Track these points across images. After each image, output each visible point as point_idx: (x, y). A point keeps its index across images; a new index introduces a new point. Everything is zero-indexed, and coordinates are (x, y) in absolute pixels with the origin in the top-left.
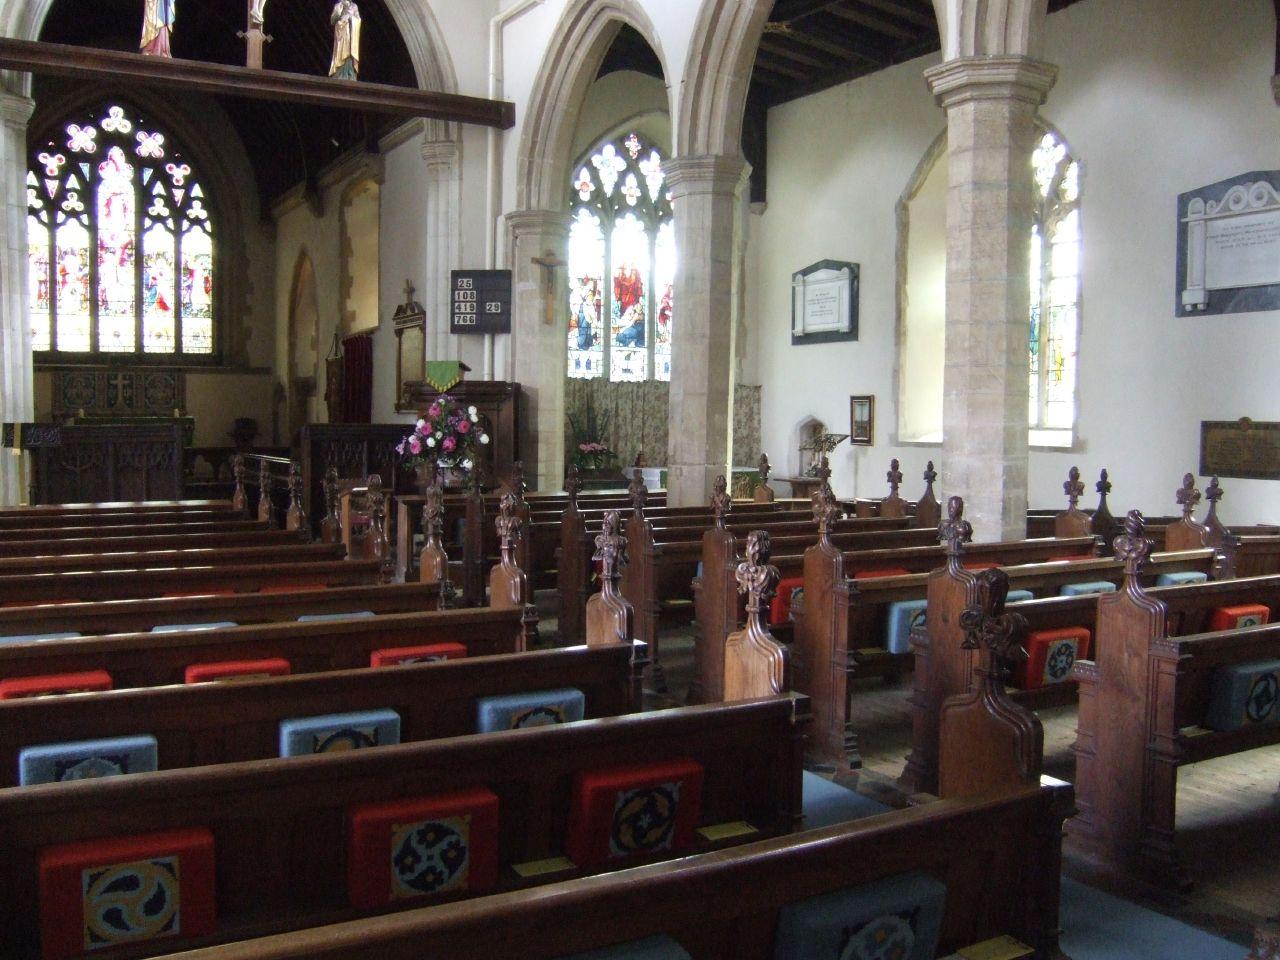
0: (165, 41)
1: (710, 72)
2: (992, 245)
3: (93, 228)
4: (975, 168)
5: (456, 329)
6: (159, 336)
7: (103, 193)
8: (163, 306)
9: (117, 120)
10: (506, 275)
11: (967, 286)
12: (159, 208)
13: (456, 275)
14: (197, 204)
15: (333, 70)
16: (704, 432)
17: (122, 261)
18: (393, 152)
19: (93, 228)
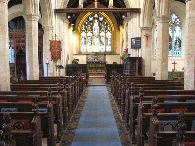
0: (82, 5)
1: (147, 3)
2: (193, 30)
3: (92, 33)
4: (189, 14)
5: (132, 48)
6: (103, 49)
7: (94, 27)
9: (96, 16)
10: (140, 38)
11: (187, 39)
12: (102, 29)
13: (132, 39)
14: (108, 28)
15: (109, 6)
16: (161, 66)
17: (97, 38)
18: (69, 24)
19: (92, 33)
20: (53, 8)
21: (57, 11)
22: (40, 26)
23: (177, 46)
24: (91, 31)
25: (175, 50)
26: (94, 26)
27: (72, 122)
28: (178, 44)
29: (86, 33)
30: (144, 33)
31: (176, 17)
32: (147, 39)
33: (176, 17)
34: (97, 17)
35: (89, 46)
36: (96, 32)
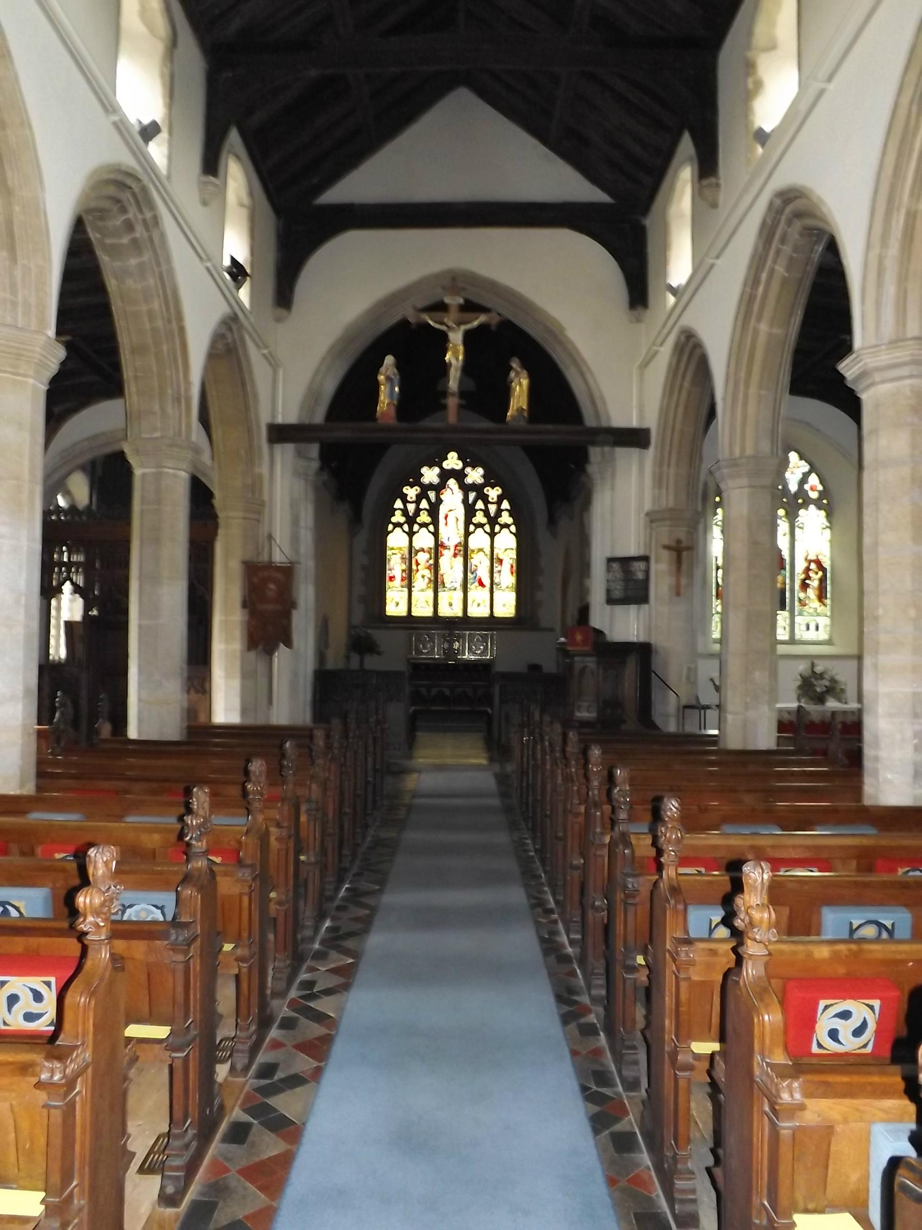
0: (393, 412)
3: (436, 534)
8: (481, 584)
9: (453, 461)
12: (480, 518)
13: (610, 560)
17: (455, 555)
19: (436, 534)
20: (265, 418)
21: (280, 434)
22: (201, 496)
23: (812, 593)
24: (431, 528)
25: (800, 614)
26: (441, 507)
27: (320, 956)
28: (815, 583)
29: (411, 534)
30: (665, 534)
31: (805, 467)
32: (679, 561)
33: (805, 467)
34: (459, 465)
35: (422, 590)
36: (451, 532)
